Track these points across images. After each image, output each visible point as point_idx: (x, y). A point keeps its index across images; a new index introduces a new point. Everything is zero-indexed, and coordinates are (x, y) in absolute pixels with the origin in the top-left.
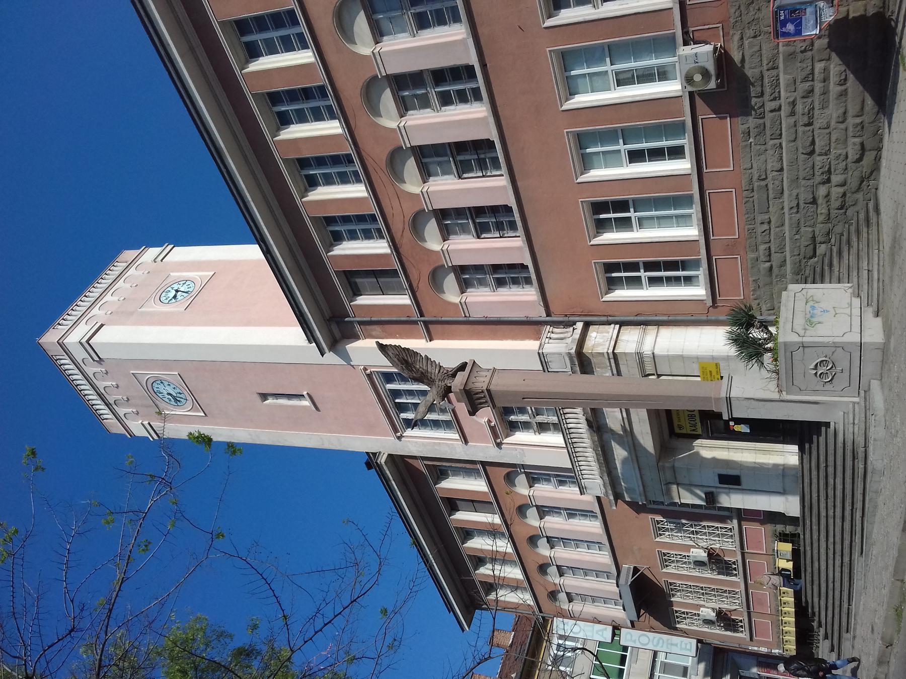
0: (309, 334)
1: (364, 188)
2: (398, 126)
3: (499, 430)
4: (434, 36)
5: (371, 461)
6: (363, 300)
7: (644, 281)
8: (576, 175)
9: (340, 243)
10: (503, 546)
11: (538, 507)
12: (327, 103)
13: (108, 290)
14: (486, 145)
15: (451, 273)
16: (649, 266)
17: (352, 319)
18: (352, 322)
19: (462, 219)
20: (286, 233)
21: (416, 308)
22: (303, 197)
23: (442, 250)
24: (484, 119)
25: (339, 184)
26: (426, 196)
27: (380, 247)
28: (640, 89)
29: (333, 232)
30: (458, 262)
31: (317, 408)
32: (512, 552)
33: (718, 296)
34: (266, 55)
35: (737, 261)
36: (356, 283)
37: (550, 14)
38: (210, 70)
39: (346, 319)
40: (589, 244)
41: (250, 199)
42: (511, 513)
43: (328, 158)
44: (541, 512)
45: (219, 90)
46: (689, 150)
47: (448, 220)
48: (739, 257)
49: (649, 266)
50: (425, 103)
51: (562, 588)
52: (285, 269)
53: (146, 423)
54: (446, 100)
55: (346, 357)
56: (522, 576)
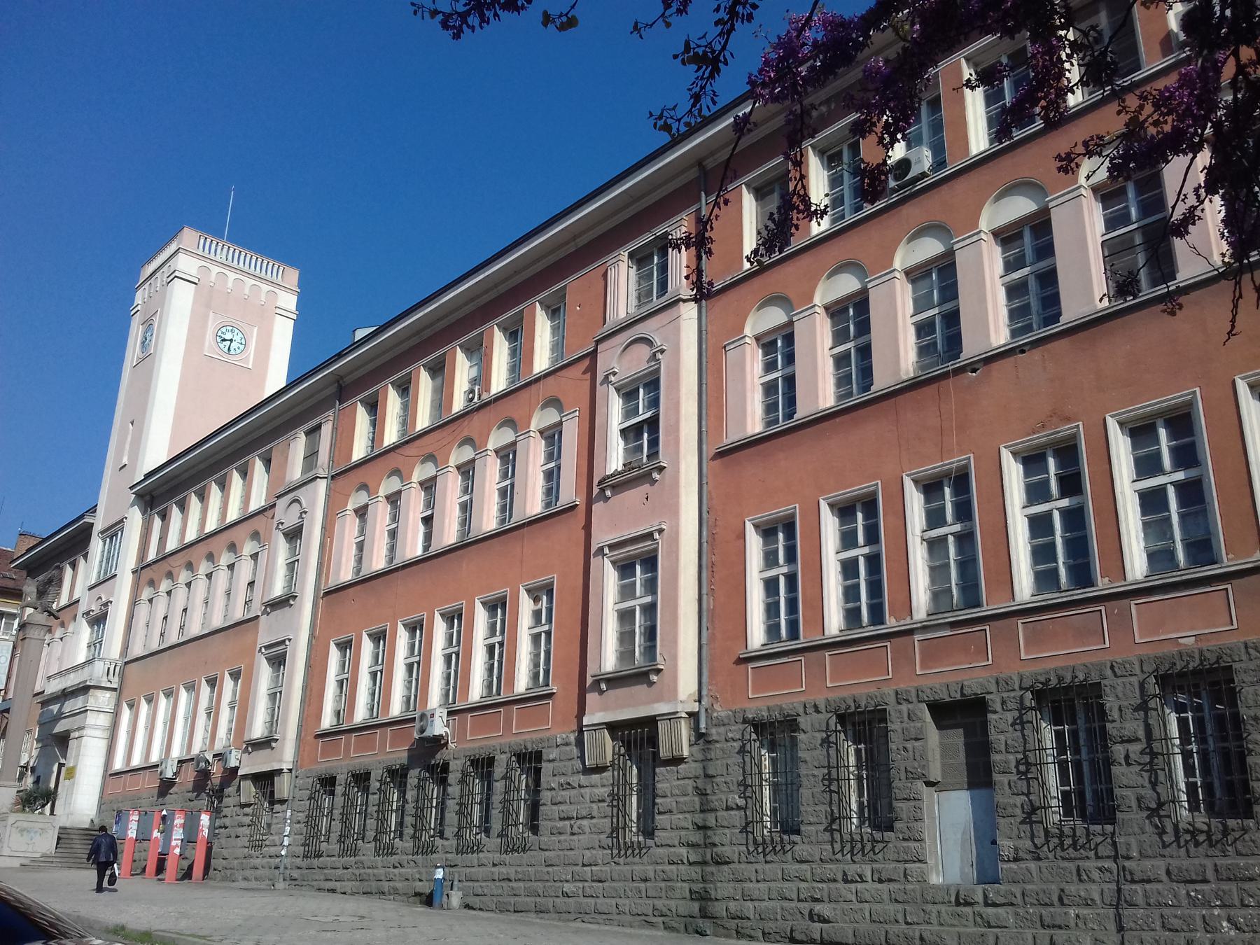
1: (982, 149)
2: (894, 270)
5: (93, 510)
6: (749, 203)
7: (771, 573)
8: (1010, 446)
10: (499, 381)
12: (847, 212)
13: (238, 272)
15: (1037, 204)
16: (874, 562)
18: (700, 200)
22: (541, 303)
23: (1081, 186)
25: (987, 113)
28: (182, 746)
29: (840, 154)
30: (1057, 217)
31: (121, 469)
32: (453, 413)
33: (1136, 602)
35: (1227, 625)
36: (772, 192)
37: (1124, 423)
38: (218, 457)
39: (703, 193)
40: (1001, 446)
41: (426, 311)
42: (507, 408)
44: (551, 432)
45: (493, 295)
46: (1051, 597)
47: (783, 343)
48: (990, 662)
49: (874, 562)
51: (443, 471)
52: (292, 394)
53: (139, 308)
54: (841, 361)
55: (132, 505)
56: (538, 372)
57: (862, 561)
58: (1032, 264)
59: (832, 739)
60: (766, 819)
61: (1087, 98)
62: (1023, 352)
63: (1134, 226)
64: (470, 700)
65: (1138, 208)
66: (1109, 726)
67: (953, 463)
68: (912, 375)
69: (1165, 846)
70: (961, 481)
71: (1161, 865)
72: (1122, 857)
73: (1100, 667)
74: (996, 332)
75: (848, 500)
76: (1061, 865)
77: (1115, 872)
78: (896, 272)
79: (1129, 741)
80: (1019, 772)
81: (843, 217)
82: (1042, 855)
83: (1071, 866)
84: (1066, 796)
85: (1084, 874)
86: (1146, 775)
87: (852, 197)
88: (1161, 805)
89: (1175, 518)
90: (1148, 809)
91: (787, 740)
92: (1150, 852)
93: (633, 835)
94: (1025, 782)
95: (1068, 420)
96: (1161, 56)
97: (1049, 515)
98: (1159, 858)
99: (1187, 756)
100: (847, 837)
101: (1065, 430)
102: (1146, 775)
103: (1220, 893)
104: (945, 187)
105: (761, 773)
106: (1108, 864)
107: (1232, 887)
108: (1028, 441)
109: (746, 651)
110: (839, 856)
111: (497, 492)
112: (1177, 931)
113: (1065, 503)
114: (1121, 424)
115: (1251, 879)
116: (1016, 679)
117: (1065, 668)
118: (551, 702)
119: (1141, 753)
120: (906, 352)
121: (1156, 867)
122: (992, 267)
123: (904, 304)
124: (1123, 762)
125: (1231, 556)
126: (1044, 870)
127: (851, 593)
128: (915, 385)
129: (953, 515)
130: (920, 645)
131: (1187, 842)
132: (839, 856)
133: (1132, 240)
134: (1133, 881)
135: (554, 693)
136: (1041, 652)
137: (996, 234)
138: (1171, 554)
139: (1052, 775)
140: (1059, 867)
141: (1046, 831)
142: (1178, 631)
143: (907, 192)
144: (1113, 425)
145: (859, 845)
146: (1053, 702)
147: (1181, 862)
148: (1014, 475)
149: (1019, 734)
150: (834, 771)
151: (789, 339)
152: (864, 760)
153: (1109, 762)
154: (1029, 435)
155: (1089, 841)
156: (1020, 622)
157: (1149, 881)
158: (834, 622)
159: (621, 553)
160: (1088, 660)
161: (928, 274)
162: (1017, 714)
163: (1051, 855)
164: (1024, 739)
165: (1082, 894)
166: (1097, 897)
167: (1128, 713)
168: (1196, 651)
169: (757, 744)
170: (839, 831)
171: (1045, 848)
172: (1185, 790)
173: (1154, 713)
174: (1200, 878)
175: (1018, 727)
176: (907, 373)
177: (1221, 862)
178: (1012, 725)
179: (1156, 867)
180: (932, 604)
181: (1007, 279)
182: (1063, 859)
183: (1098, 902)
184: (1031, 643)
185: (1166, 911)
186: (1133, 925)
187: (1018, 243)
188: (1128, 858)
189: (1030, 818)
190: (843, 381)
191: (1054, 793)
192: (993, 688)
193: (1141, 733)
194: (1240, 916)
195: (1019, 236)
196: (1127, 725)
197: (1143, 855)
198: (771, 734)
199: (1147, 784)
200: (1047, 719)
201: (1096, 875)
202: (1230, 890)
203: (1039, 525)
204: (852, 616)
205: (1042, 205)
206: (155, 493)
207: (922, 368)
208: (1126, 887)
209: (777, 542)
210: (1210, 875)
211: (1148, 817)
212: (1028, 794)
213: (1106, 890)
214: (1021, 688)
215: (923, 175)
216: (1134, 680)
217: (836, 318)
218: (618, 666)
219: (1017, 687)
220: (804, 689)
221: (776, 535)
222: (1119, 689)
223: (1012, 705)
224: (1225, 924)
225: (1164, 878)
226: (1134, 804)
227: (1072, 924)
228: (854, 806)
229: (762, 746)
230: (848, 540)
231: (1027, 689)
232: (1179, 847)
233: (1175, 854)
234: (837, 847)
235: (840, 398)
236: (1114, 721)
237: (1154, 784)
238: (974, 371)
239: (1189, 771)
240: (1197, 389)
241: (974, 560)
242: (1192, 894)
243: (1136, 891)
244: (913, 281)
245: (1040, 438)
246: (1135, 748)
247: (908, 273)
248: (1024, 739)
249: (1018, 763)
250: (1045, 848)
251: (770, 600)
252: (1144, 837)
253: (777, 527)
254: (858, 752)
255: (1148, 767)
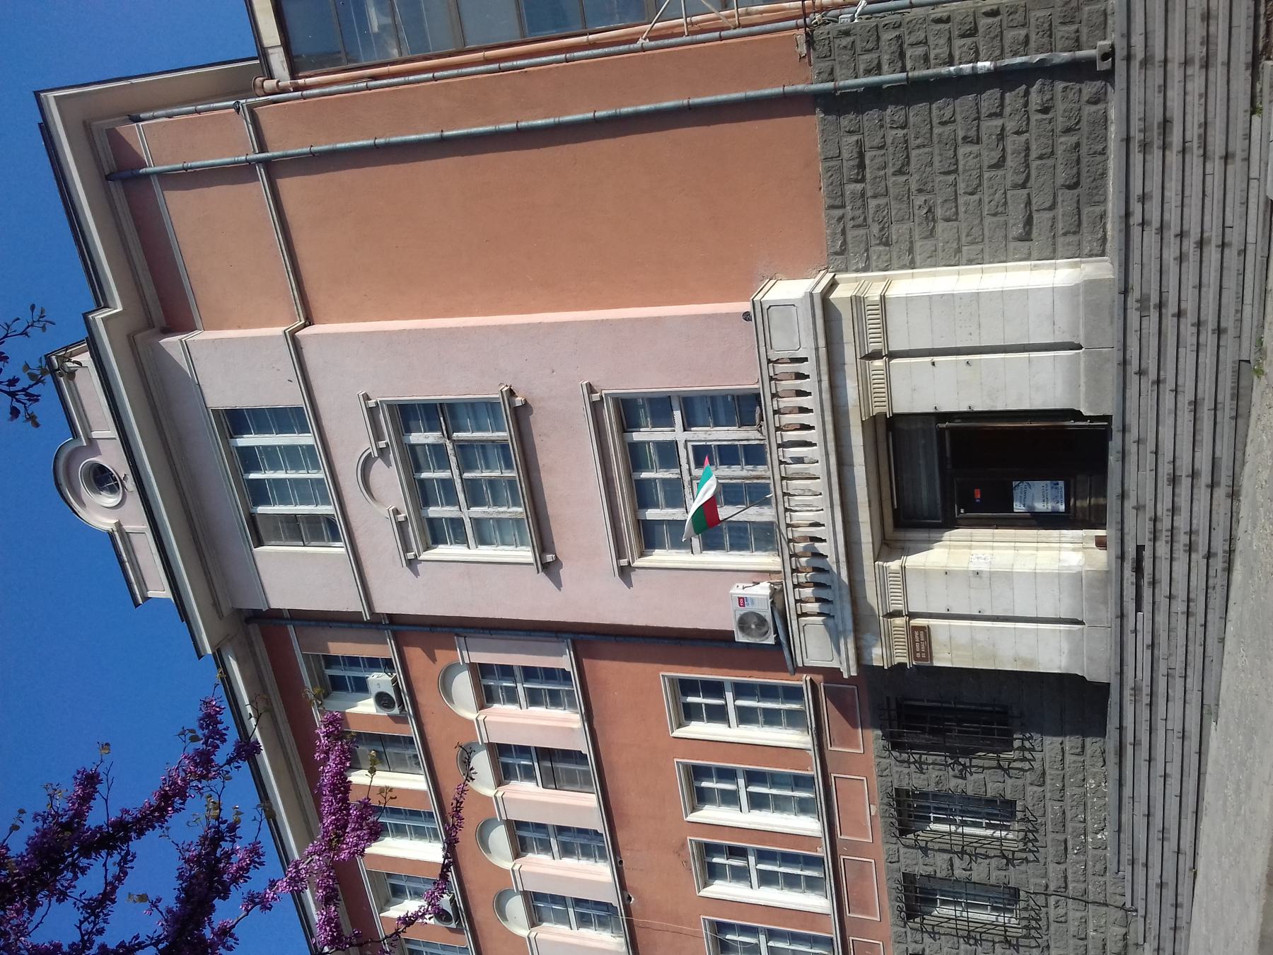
0: (260, 789)
3: (413, 531)
4: (394, 77)
8: (699, 889)
9: (399, 900)
11: (525, 894)
14: (574, 756)
17: (148, 170)
18: (148, 175)
19: (507, 681)
20: (148, 297)
21: (271, 203)
24: (610, 883)
26: (517, 875)
27: (416, 782)
34: (353, 691)
39: (141, 171)
43: (302, 449)
50: (512, 697)
54: (534, 699)
57: (740, 703)
58: (548, 835)
59: (923, 844)
60: (998, 834)
61: (422, 772)
62: (621, 862)
63: (536, 764)
64: (829, 911)
65: (502, 679)
66: (938, 875)
67: (706, 934)
68: (623, 940)
69: (1037, 860)
70: (698, 773)
71: (1052, 867)
72: (1046, 890)
73: (889, 870)
74: (599, 874)
75: (691, 795)
76: (1053, 932)
77: (1058, 898)
78: (497, 795)
79: (952, 865)
80: (975, 944)
81: (435, 829)
82: (1046, 944)
83: (1053, 927)
84: (994, 909)
85: (1061, 919)
86: (979, 860)
87: (420, 818)
88: (1004, 857)
89: (774, 791)
90: (1007, 865)
91: (865, 57)
92: (1043, 871)
93: (1011, 836)
94: (983, 943)
95: (684, 845)
96: (386, 646)
97: (760, 872)
98: (1047, 866)
99: (964, 824)
100: (1021, 845)
101: (691, 849)
102: (979, 860)
103: (1075, 834)
104: (467, 886)
105: (950, 833)
106: (1052, 900)
107: (1070, 826)
108: (697, 876)
109: (823, 839)
110: (1036, 765)
111: (582, 930)
112: (1106, 868)
113: (729, 695)
114: (680, 726)
115: (1064, 813)
116: (896, 929)
117: (889, 894)
118: (842, 857)
119: (962, 860)
120: (602, 941)
121: (1054, 871)
122: (528, 793)
123: (560, 934)
124: (969, 873)
125: (809, 768)
126: (1058, 945)
127: (771, 718)
128: (588, 717)
129: (751, 937)
130: (836, 746)
131: (1034, 846)
132: (1036, 765)
133: (546, 768)
134: (1066, 887)
135: (811, 679)
136: (875, 906)
137: (481, 707)
138: (801, 800)
139: (975, 915)
140: (1055, 934)
141: (1025, 937)
142: (866, 815)
143: (463, 916)
144: (679, 733)
145: (1033, 931)
146: (917, 902)
147: (1050, 851)
148: (699, 729)
149: (943, 937)
150: (960, 933)
151: (538, 896)
152: (940, 704)
153: (968, 881)
154: (692, 873)
155: (1033, 909)
156: (829, 748)
157: (1066, 877)
158: (818, 903)
159: (630, 538)
160: (884, 877)
161: (537, 909)
162: (926, 935)
163: (1045, 938)
164: (947, 934)
165: (1077, 924)
166: (1079, 914)
167: (931, 861)
168: (882, 807)
169: (920, 833)
170: (1014, 852)
171: (1039, 941)
172: (992, 831)
173: (929, 844)
174: (1063, 844)
175: (937, 936)
176: (620, 944)
177: (1050, 828)
178: (935, 940)
179: (1054, 871)
180: (817, 892)
181: (557, 855)
182: (1048, 929)
183: (1083, 914)
184: (865, 908)
185: (1090, 871)
186: (1101, 895)
187: (528, 841)
188: (1047, 886)
189: (1014, 946)
190: (555, 699)
191: (994, 918)
192: (904, 946)
193: (946, 856)
194: (1092, 825)
195: (488, 688)
196: (939, 863)
197: (1045, 876)
198: (910, 816)
199: (988, 861)
200: (931, 909)
201: (1061, 911)
202: (1073, 828)
203: (746, 716)
204: (794, 720)
205: (484, 747)
206: (109, 164)
207: (618, 927)
208: (1070, 892)
209: (712, 789)
210: (1061, 837)
211: (1014, 866)
212: (994, 943)
213: (1074, 907)
214: (905, 927)
215: (395, 680)
216: (902, 850)
217: (544, 917)
218: (821, 893)
219: (903, 930)
220: (865, 779)
221: (703, 788)
222: (909, 861)
223: (918, 936)
224: (1099, 836)
225: (1063, 867)
226: (1003, 873)
227: (1102, 936)
228: (989, 832)
229: (930, 914)
230: (730, 799)
231: (905, 923)
232: (1038, 851)
233: (1044, 855)
234: (1026, 766)
235: (572, 705)
236: (935, 872)
237: (987, 857)
238: (630, 899)
239: (978, 825)
240: (675, 760)
241: (772, 775)
242: (1076, 851)
243: (1074, 887)
244: (541, 920)
245: (695, 866)
246: (957, 861)
247: (533, 924)
248: (947, 934)
249: (967, 943)
250: (1039, 941)
251: (761, 718)
252: (1030, 872)
253: (708, 863)
254: (937, 820)
255: (974, 858)
